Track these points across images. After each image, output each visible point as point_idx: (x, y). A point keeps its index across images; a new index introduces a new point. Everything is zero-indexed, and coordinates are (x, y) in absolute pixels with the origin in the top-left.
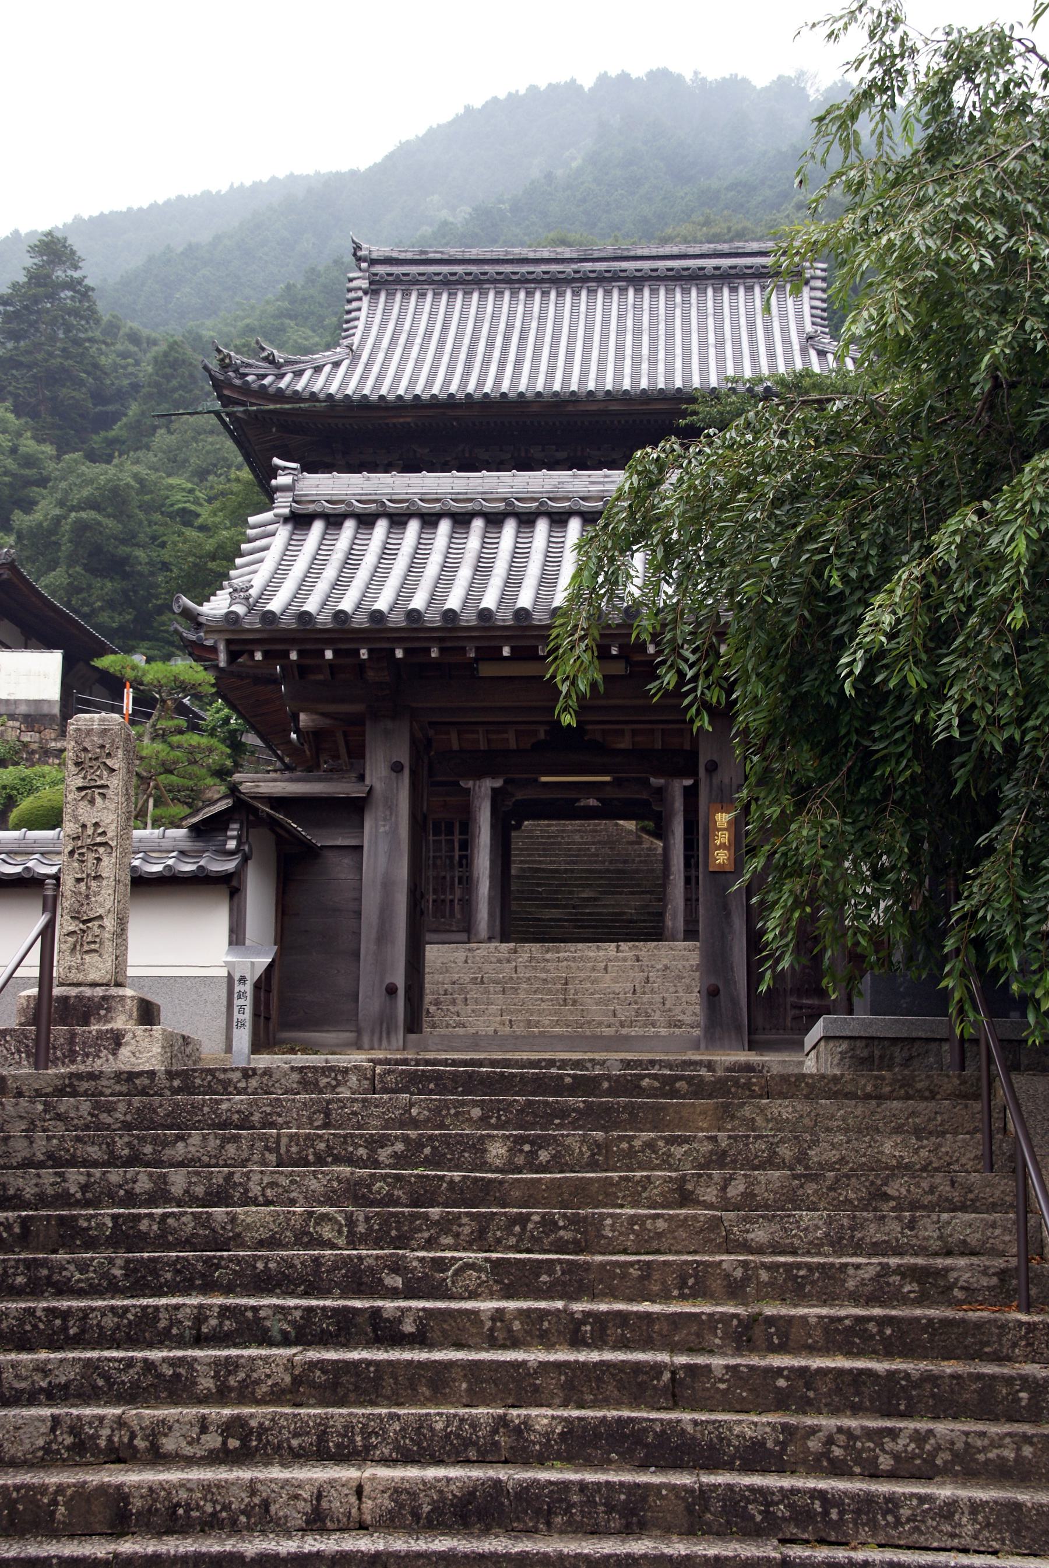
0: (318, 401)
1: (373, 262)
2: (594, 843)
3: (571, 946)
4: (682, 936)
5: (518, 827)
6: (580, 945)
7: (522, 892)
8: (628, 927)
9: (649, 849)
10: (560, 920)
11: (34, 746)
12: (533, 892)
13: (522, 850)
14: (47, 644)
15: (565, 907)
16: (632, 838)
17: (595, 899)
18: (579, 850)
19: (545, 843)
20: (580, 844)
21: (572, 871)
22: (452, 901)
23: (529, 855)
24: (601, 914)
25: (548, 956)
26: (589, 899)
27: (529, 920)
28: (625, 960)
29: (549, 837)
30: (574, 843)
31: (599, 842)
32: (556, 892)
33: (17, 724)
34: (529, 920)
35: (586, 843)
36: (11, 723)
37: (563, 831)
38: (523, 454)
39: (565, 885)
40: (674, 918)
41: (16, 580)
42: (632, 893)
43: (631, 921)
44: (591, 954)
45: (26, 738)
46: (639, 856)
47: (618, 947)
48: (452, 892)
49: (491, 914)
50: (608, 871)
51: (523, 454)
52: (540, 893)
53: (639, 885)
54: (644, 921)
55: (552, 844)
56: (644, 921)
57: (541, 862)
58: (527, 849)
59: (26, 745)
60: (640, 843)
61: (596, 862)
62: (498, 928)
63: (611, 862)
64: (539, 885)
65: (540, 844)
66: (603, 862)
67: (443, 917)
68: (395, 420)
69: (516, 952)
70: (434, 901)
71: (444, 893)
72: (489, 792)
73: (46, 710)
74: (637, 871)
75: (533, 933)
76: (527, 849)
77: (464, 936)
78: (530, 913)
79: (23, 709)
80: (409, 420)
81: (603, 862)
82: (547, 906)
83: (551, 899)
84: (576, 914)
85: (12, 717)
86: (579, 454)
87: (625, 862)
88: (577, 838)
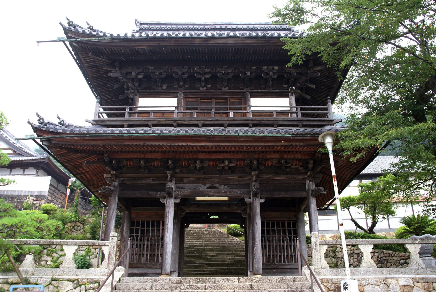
0: (106, 37)
1: (141, 24)
2: (213, 238)
3: (213, 279)
4: (261, 271)
5: (187, 226)
6: (217, 279)
7: (189, 253)
8: (228, 266)
9: (232, 240)
10: (203, 263)
11: (37, 205)
12: (193, 253)
13: (190, 240)
14: (49, 174)
15: (205, 259)
16: (226, 236)
17: (215, 256)
18: (209, 240)
19: (198, 238)
20: (209, 238)
21: (207, 246)
22: (158, 255)
23: (192, 241)
24: (217, 261)
25: (199, 285)
26: (213, 256)
27: (191, 263)
28: (244, 287)
29: (199, 236)
30: (207, 238)
31: (215, 237)
32: (201, 253)
33: (33, 198)
34: (191, 263)
35: (211, 238)
36: (31, 198)
37: (203, 234)
38: (192, 71)
39: (204, 251)
40: (258, 263)
41: (50, 163)
42: (228, 254)
43: (229, 264)
44: (225, 284)
45: (35, 202)
46: (229, 242)
47: (239, 279)
48: (158, 251)
49: (173, 261)
50: (219, 246)
51: (192, 71)
52: (196, 254)
53: (230, 251)
54: (233, 264)
55: (200, 238)
56: (233, 264)
57: (196, 244)
58: (192, 240)
59: (35, 204)
60: (229, 238)
61: (214, 244)
62: (177, 267)
63: (219, 244)
64: (195, 251)
65: (196, 238)
66: (217, 244)
67: (154, 262)
68: (138, 48)
69: (181, 282)
70: (150, 255)
71: (154, 251)
72: (173, 205)
73: (43, 194)
74: (229, 246)
75: (193, 268)
76: (192, 240)
77: (159, 271)
78: (192, 261)
79: (36, 194)
80: (144, 47)
81: (217, 244)
82: (198, 258)
83: (200, 256)
84: (208, 261)
85: (32, 196)
86: (214, 71)
87: (224, 244)
88: (208, 236)
